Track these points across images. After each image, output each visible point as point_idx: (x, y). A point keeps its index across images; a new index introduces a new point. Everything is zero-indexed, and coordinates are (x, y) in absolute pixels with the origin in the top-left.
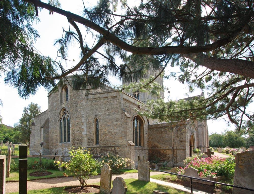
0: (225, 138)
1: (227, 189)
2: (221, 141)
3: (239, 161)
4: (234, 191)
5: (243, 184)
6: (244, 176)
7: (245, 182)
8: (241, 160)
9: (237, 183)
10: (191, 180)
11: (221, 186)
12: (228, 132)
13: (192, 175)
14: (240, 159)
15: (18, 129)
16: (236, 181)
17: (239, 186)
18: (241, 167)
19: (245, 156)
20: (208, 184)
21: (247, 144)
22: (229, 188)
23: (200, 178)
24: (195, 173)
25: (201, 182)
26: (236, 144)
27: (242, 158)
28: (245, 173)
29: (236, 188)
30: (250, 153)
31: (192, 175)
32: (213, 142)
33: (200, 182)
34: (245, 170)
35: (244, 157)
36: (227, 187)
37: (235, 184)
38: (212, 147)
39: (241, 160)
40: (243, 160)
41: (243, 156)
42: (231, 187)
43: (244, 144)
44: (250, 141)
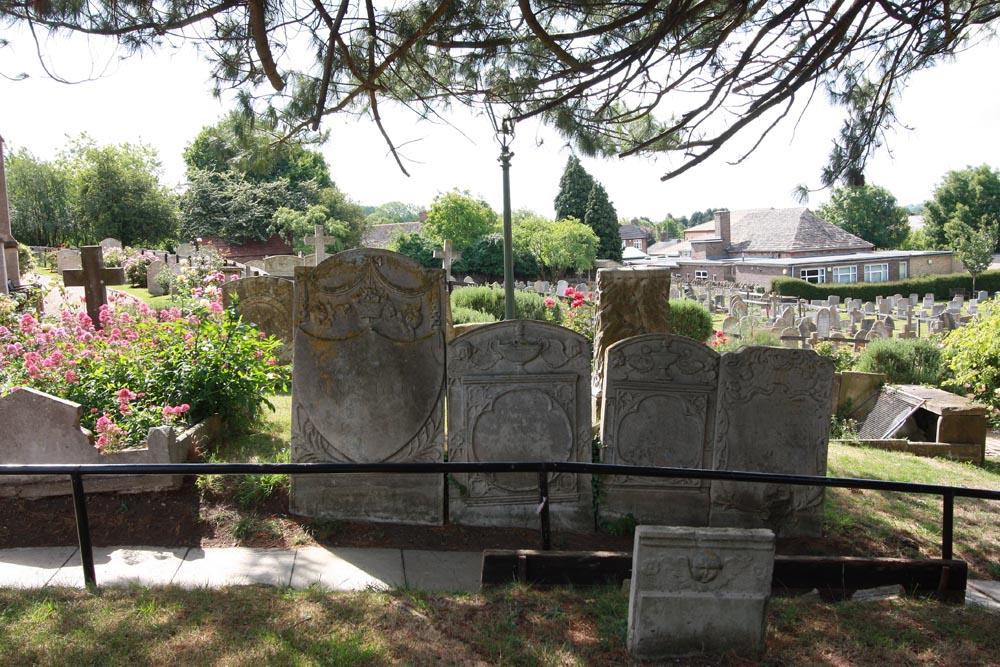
0: (85, 190)
1: (262, 491)
2: (63, 204)
3: (308, 315)
4: (300, 494)
5: (335, 441)
6: (337, 396)
7: (343, 429)
8: (321, 307)
9: (308, 446)
10: (78, 486)
11: (228, 481)
12: (93, 156)
13: (34, 447)
14: (312, 303)
15: (28, 602)
16: (305, 432)
17: (322, 458)
18: (322, 347)
19: (336, 284)
20: (157, 489)
21: (189, 222)
22: (272, 481)
23: (101, 459)
24: (58, 432)
25: (109, 488)
26: (140, 227)
27: (321, 296)
28: (341, 377)
29: (302, 477)
30: (354, 262)
31: (34, 447)
32: (14, 210)
33: (100, 489)
34: (340, 363)
35: (332, 290)
36: (262, 478)
37: (300, 451)
38: (27, 244)
39: (321, 307)
40: (328, 306)
41: (323, 282)
42: (276, 477)
43: (175, 227)
44: (197, 210)
